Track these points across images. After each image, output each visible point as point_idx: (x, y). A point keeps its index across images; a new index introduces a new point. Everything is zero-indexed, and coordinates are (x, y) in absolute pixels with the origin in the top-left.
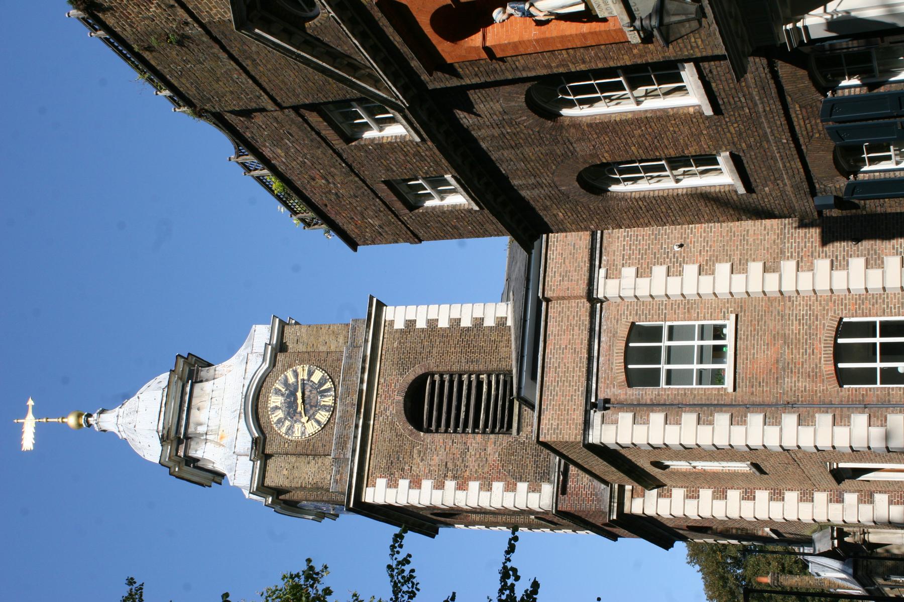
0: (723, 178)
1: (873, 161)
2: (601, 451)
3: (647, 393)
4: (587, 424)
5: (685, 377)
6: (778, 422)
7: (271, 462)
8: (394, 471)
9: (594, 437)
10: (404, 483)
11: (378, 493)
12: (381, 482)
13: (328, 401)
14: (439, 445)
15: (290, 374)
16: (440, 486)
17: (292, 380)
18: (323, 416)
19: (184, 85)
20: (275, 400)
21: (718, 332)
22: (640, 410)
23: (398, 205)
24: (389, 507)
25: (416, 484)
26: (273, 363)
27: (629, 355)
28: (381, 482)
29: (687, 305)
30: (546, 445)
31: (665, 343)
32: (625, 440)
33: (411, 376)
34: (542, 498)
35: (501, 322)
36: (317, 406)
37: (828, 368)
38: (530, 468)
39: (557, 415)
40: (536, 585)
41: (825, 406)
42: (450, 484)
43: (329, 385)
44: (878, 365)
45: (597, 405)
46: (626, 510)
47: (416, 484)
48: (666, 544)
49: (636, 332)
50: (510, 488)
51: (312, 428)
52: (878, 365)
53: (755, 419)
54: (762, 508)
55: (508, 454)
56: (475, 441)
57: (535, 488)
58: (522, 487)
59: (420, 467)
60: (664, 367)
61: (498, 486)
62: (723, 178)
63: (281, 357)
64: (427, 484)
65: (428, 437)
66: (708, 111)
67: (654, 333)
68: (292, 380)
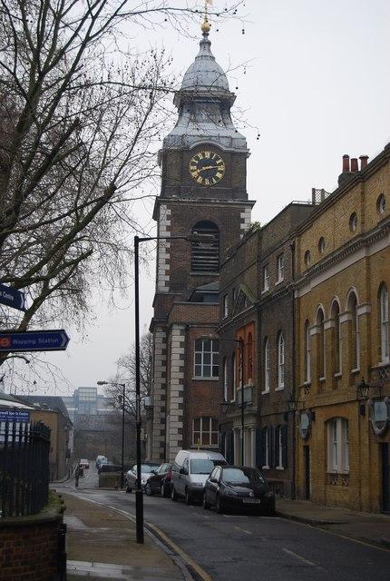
4: (181, 324)
13: (207, 182)
20: (208, 155)
22: (185, 345)
45: (187, 331)
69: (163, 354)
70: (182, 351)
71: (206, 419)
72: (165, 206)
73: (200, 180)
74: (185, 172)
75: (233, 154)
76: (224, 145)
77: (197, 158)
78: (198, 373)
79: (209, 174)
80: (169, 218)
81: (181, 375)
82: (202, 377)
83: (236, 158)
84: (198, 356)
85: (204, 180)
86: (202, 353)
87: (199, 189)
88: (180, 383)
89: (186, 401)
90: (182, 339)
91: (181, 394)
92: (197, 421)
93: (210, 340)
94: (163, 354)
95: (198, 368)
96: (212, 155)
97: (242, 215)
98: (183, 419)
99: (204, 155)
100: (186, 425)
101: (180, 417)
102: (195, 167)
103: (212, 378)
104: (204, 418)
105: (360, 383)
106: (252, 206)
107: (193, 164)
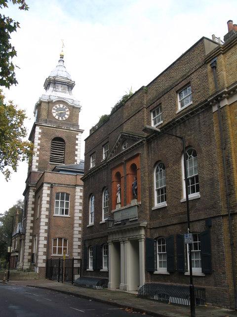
0: (91, 223)
1: (91, 253)
2: (42, 186)
3: (55, 197)
4: (49, 183)
5: (57, 205)
6: (46, 225)
7: (47, 104)
8: (43, 134)
9: (45, 185)
10: (40, 136)
11: (38, 130)
12: (40, 131)
13: (60, 119)
14: (48, 145)
15: (68, 110)
16: (39, 145)
17: (66, 110)
18: (57, 117)
19: (94, 135)
20: (61, 106)
21: (67, 213)
22: (50, 195)
23: (91, 153)
24: (35, 133)
25: (39, 139)
26: (70, 106)
27: (63, 194)
28: (40, 131)
29: (73, 207)
30: (44, 174)
31: (65, 201)
32: (44, 191)
33: (65, 139)
34: (34, 169)
35: (76, 161)
36: (59, 116)
37: (57, 236)
38: (41, 166)
39: (50, 177)
40: (7, 181)
41: (49, 235)
42: (39, 147)
43: (64, 119)
44: (57, 247)
45: (52, 187)
46: (30, 188)
47: (39, 139)
48: (24, 194)
49: (68, 195)
50: (37, 161)
51: (54, 115)
52: (57, 247)
53: (47, 220)
54: (30, 218)
55: (45, 161)
56: (49, 153)
57: (37, 167)
58: (37, 164)
59: (43, 140)
60: (60, 201)
61: (38, 158)
62: (91, 223)
63: (72, 108)
64: (39, 142)
65: (50, 142)
66: (101, 223)
67: (67, 199)
68: (66, 110)
69: (30, 248)
70: (48, 199)
71: (60, 239)
72: (39, 128)
73: (60, 119)
74: (49, 113)
75: (74, 107)
76: (70, 102)
77: (56, 107)
78: (55, 252)
79: (61, 115)
80: (40, 133)
81: (47, 213)
82: (59, 215)
83: (75, 110)
84: (57, 203)
85: (59, 118)
86: (60, 201)
87: (57, 121)
88: (44, 247)
89: (49, 228)
90: (49, 192)
91: (46, 238)
92: (55, 240)
93: (62, 239)
94: (30, 248)
95: (55, 249)
96: (63, 107)
97: (77, 137)
98: (48, 239)
99: (60, 106)
100: (48, 242)
101: (44, 252)
102: (55, 111)
103: (64, 215)
104: (59, 238)
105: (54, 92)
106: (82, 132)
107: (54, 109)
